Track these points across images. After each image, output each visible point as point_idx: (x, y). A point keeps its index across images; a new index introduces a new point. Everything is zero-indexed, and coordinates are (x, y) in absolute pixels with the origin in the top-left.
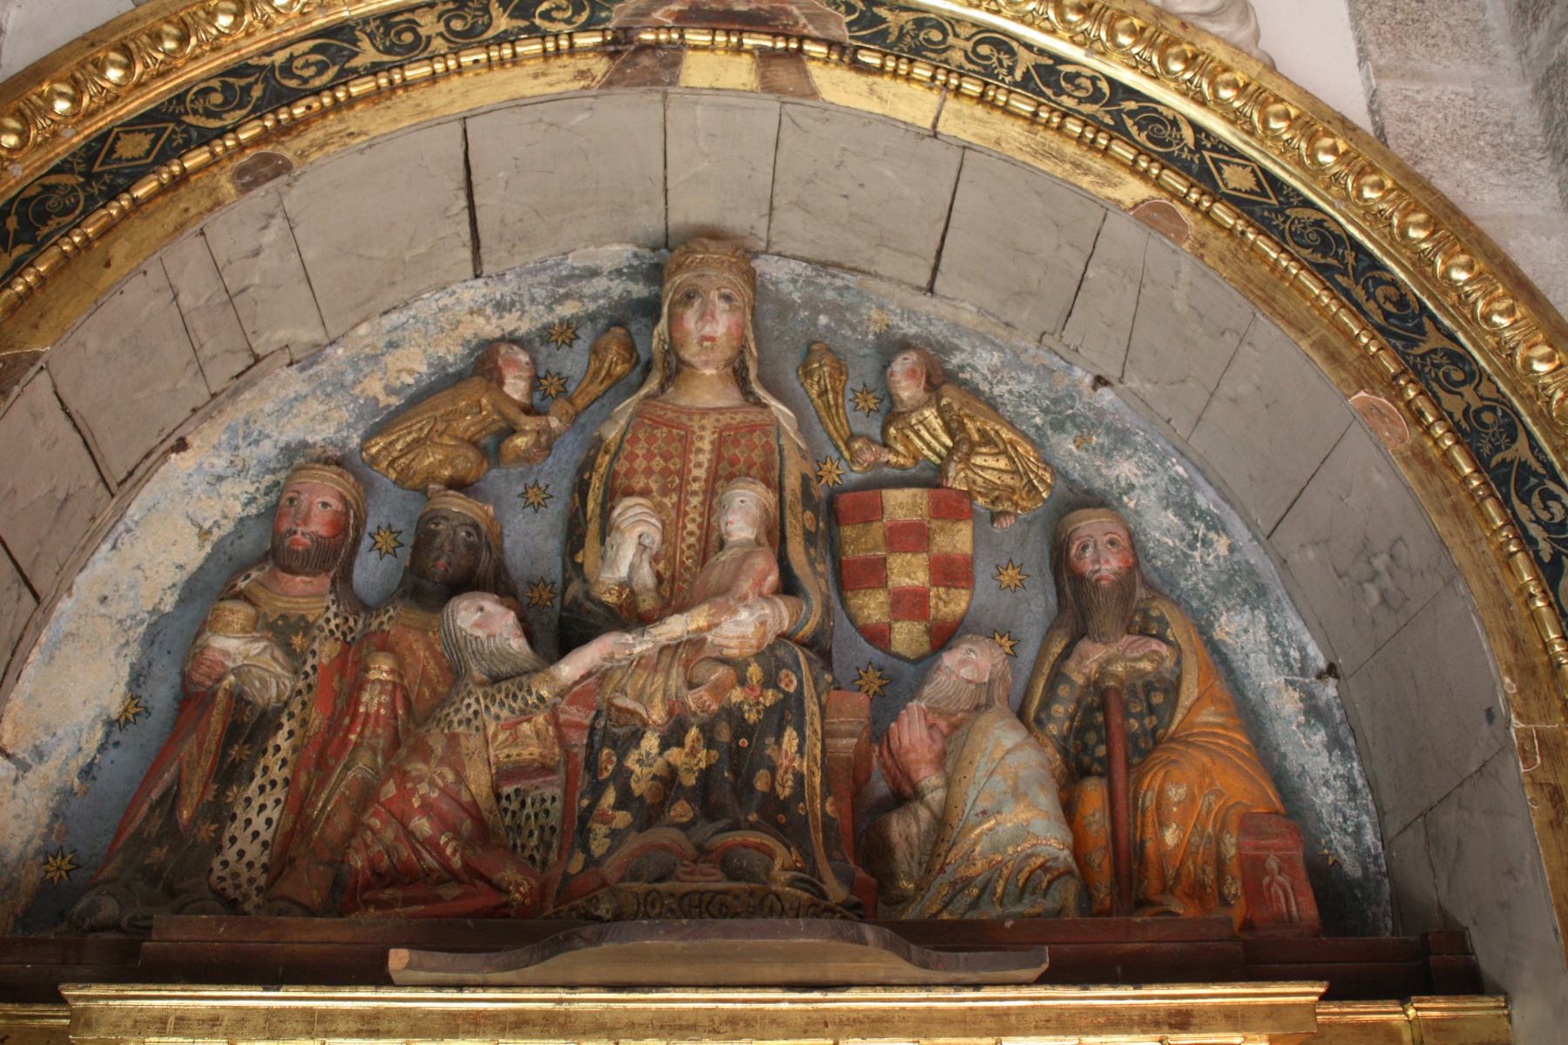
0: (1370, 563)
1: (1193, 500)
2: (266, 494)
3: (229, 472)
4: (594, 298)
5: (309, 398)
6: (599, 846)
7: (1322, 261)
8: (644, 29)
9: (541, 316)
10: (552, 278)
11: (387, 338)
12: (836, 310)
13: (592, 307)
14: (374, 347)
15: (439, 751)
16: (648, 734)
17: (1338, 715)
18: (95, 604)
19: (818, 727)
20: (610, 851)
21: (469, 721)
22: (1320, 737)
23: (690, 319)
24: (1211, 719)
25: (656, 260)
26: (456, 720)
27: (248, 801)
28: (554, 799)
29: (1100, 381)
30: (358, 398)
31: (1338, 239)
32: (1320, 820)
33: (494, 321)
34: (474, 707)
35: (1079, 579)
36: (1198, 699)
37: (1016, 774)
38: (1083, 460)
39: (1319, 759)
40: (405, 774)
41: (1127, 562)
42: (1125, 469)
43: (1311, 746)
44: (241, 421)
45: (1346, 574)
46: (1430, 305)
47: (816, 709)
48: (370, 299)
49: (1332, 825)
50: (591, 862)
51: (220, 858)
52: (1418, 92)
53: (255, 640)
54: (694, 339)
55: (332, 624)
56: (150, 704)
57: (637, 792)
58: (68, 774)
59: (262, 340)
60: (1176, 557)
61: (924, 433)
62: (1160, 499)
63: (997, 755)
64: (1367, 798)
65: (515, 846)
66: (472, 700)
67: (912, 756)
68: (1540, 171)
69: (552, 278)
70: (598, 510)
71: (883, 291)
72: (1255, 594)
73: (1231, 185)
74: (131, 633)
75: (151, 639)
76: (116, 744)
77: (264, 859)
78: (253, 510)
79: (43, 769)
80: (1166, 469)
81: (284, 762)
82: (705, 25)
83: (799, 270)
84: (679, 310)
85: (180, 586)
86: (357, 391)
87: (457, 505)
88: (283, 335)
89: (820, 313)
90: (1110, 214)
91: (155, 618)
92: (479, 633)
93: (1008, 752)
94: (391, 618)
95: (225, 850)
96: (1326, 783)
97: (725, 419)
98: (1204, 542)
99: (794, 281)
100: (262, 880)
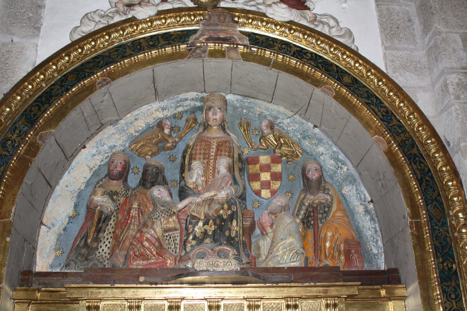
0: (379, 176)
1: (338, 157)
2: (106, 159)
3: (97, 153)
4: (187, 106)
5: (116, 134)
6: (188, 249)
7: (368, 102)
8: (198, 43)
9: (173, 111)
10: (176, 101)
11: (135, 118)
12: (248, 108)
13: (186, 109)
14: (131, 120)
15: (150, 226)
16: (200, 222)
17: (373, 212)
18: (65, 187)
19: (241, 219)
20: (191, 250)
21: (157, 218)
22: (368, 218)
23: (210, 114)
24: (339, 215)
25: (202, 96)
26: (154, 218)
27: (104, 237)
28: (178, 236)
29: (315, 126)
30: (128, 133)
31: (372, 96)
32: (367, 239)
33: (161, 113)
34: (158, 215)
35: (308, 179)
36: (337, 209)
37: (290, 230)
38: (310, 147)
39: (368, 223)
40: (142, 231)
41: (320, 175)
42: (321, 149)
43: (366, 220)
44: (99, 140)
45: (374, 178)
46: (395, 113)
47: (241, 215)
48: (130, 108)
49: (370, 240)
50: (186, 253)
51: (98, 251)
52: (396, 54)
53: (105, 197)
54: (211, 119)
55: (123, 193)
56: (79, 212)
57: (197, 236)
58: (60, 230)
59: (104, 120)
60: (333, 172)
61: (270, 141)
62: (330, 157)
63: (286, 225)
64: (379, 233)
65: (169, 248)
66: (158, 213)
67: (265, 225)
68: (426, 75)
69: (176, 101)
70: (188, 163)
71: (260, 103)
72: (353, 181)
73: (345, 82)
74: (74, 194)
75: (79, 196)
76: (71, 222)
77: (109, 251)
78: (102, 163)
79: (54, 229)
80: (332, 149)
81: (113, 227)
82: (213, 41)
83: (239, 98)
84: (208, 112)
85: (85, 183)
86: (127, 132)
87: (153, 163)
88: (109, 119)
89: (244, 109)
90: (315, 89)
91: (80, 191)
92: (159, 196)
93: (288, 224)
94: (137, 191)
95: (99, 249)
96: (369, 230)
97: (219, 140)
98: (340, 168)
99: (237, 101)
100: (108, 257)
